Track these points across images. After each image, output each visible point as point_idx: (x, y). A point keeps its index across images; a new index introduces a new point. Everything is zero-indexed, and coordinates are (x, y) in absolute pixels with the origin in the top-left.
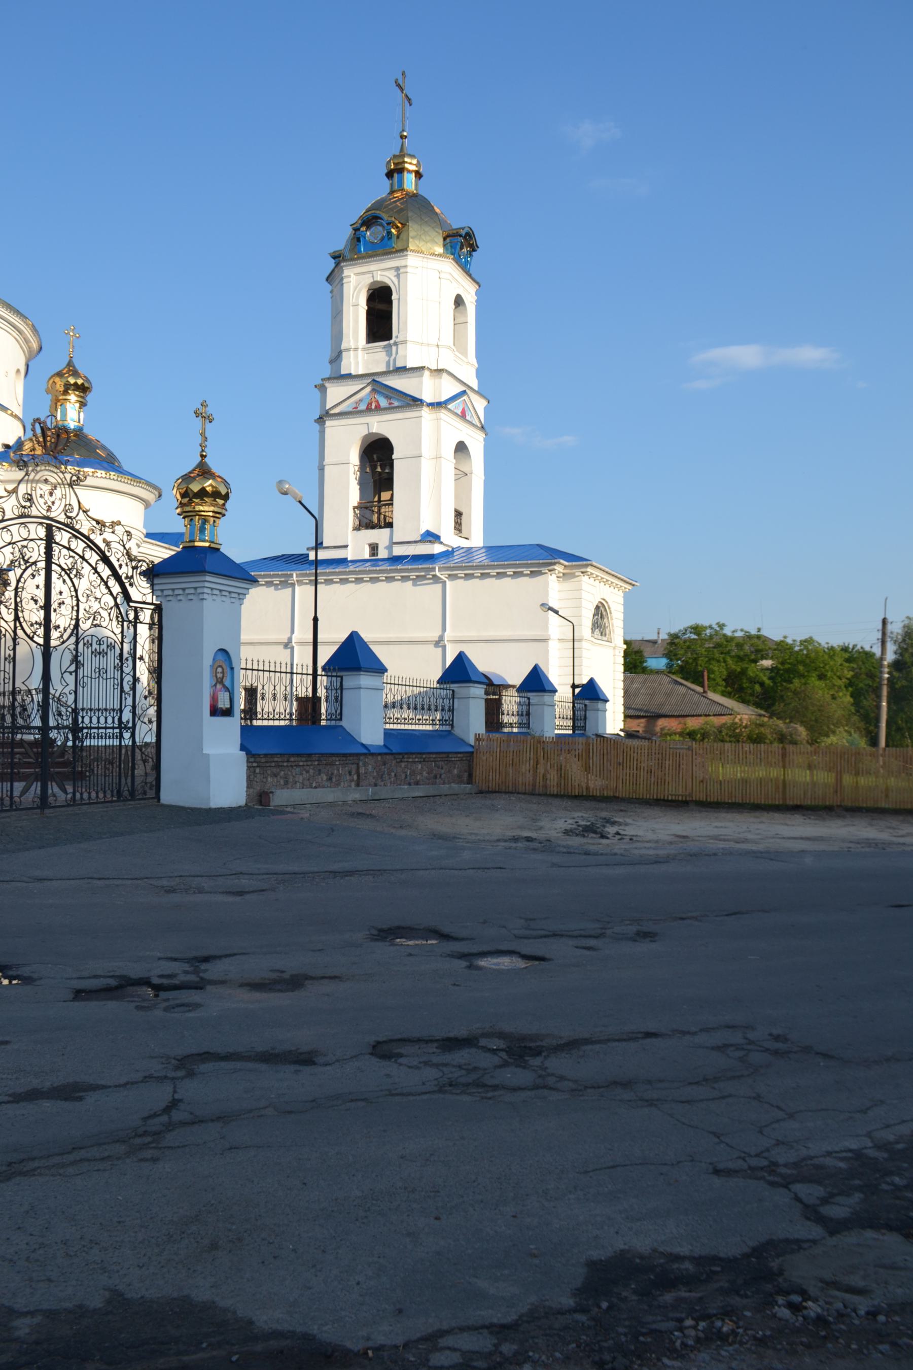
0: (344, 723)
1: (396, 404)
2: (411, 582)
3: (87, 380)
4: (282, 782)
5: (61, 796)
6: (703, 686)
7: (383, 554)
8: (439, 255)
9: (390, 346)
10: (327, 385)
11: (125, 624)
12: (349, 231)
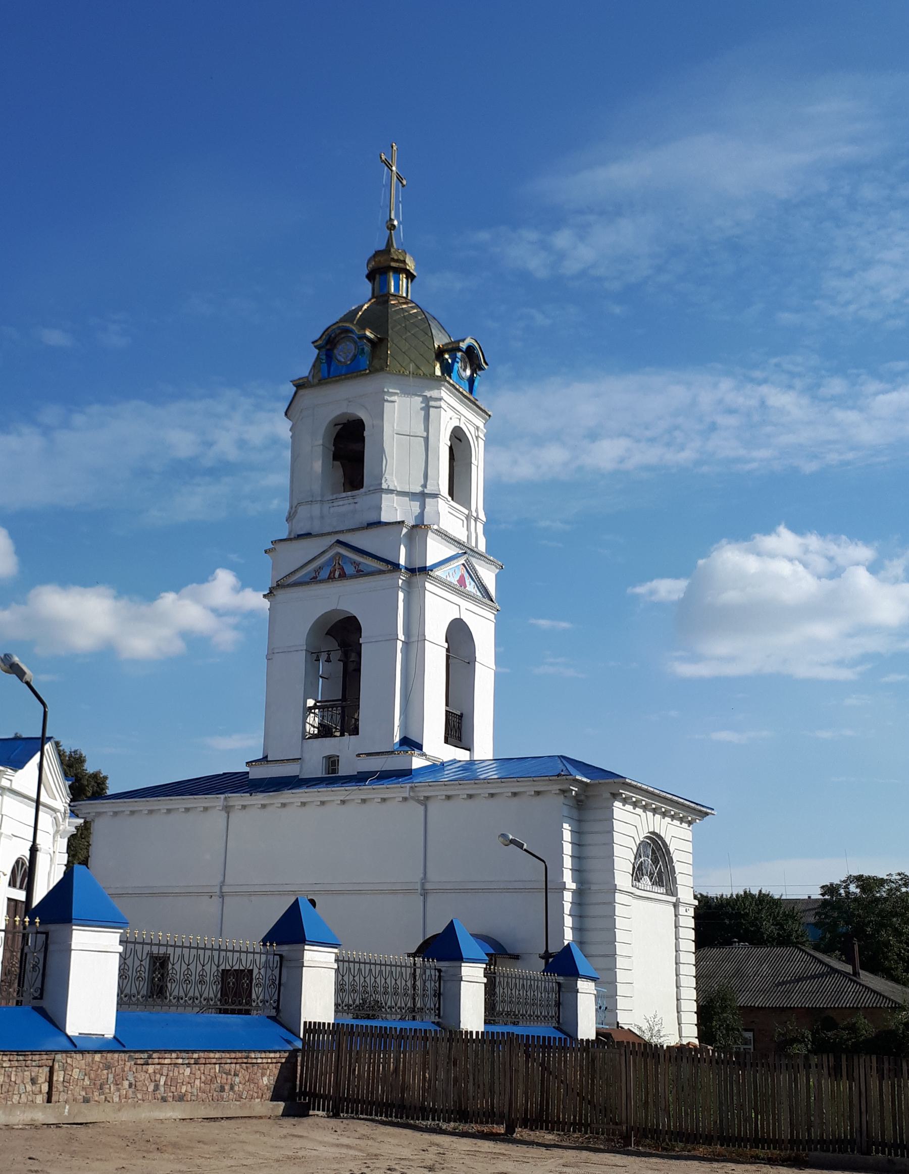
6: (850, 960)
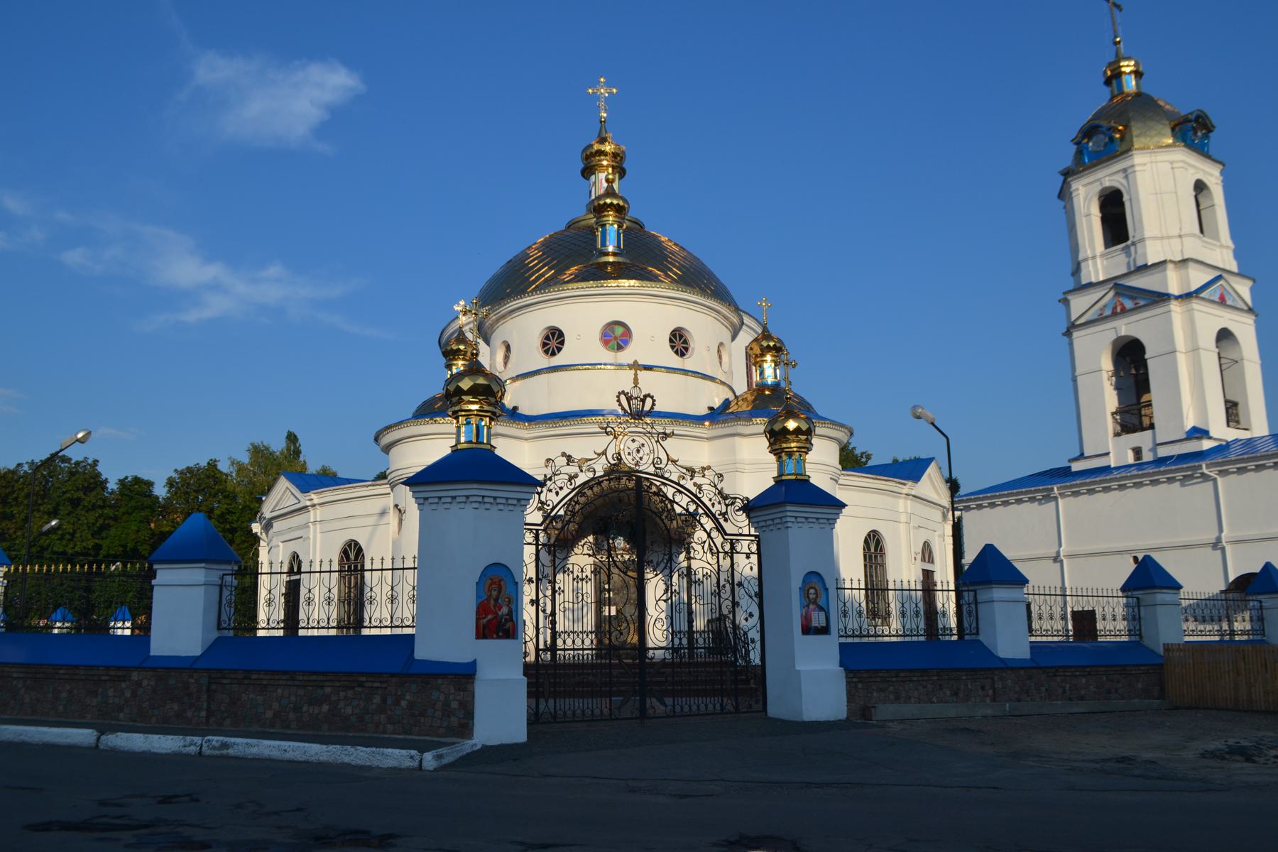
0: (981, 638)
1: (1142, 303)
2: (1177, 484)
3: (780, 341)
4: (892, 697)
5: (661, 709)
7: (1147, 457)
8: (1168, 146)
9: (1128, 247)
10: (1069, 297)
11: (721, 555)
12: (1074, 148)
